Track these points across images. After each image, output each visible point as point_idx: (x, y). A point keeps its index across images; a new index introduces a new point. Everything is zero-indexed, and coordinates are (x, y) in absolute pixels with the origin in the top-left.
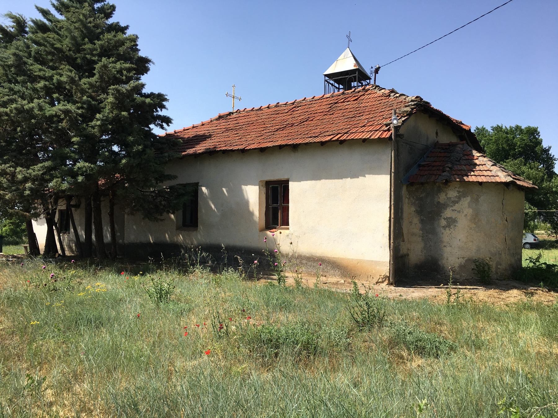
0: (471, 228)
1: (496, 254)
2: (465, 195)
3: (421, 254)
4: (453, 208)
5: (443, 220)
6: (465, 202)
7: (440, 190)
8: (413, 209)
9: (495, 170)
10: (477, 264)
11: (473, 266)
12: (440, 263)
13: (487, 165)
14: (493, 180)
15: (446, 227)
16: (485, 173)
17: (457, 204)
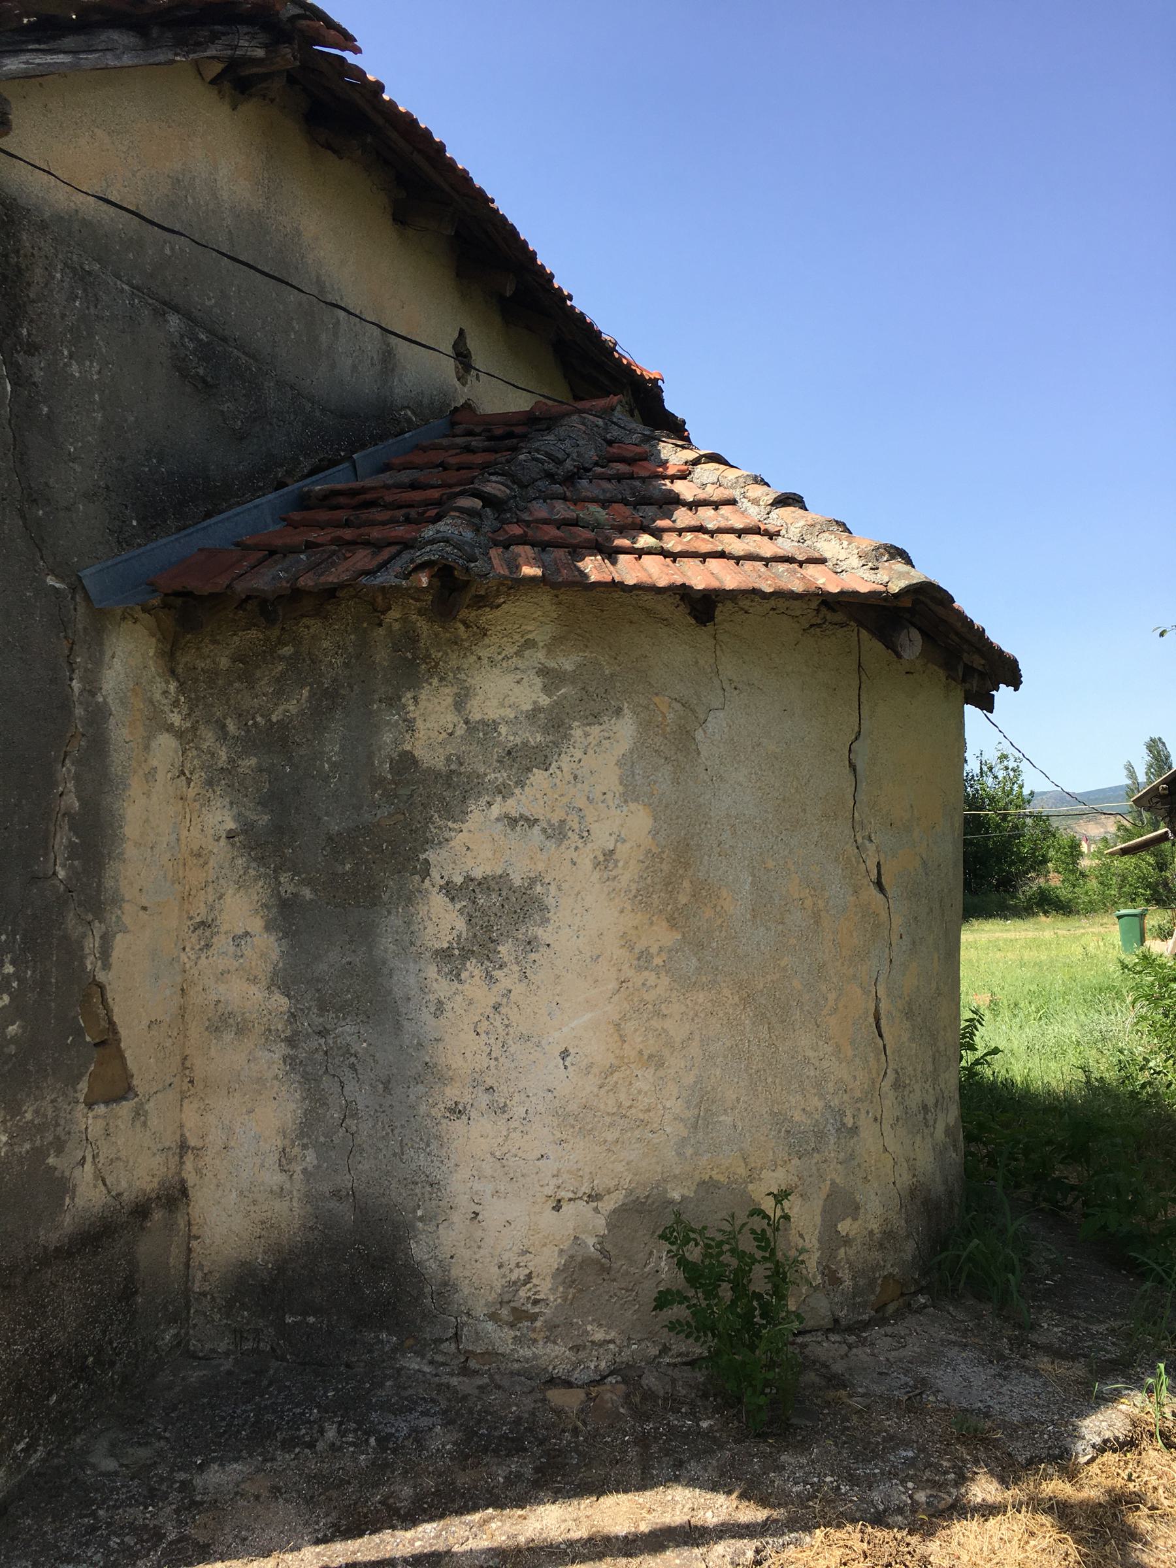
0: (643, 959)
1: (821, 1135)
2: (595, 703)
3: (275, 1178)
4: (512, 806)
5: (438, 901)
6: (602, 753)
7: (413, 667)
8: (220, 818)
9: (794, 531)
10: (694, 1253)
11: (663, 1268)
12: (418, 1250)
13: (744, 504)
14: (792, 580)
15: (466, 954)
16: (736, 545)
17: (538, 777)
